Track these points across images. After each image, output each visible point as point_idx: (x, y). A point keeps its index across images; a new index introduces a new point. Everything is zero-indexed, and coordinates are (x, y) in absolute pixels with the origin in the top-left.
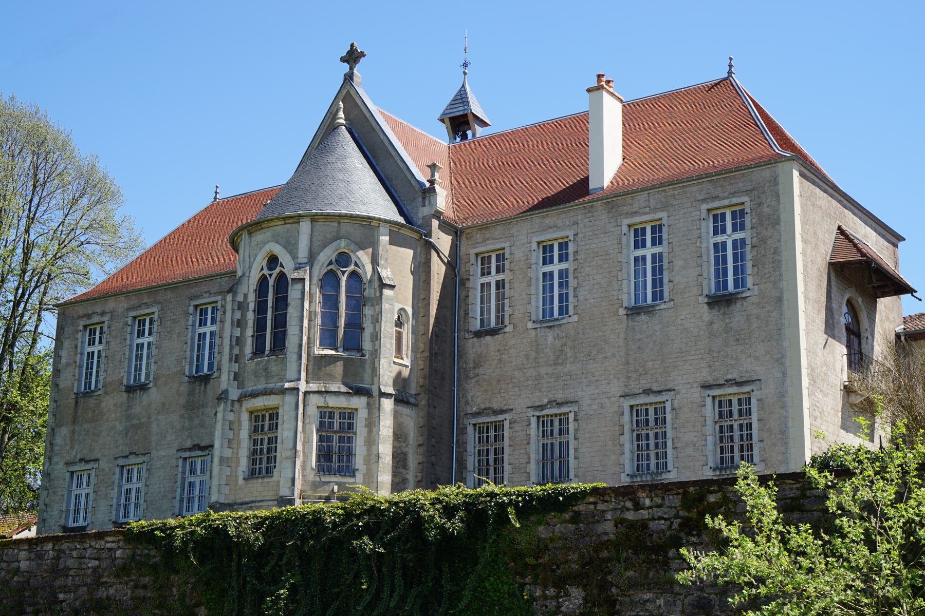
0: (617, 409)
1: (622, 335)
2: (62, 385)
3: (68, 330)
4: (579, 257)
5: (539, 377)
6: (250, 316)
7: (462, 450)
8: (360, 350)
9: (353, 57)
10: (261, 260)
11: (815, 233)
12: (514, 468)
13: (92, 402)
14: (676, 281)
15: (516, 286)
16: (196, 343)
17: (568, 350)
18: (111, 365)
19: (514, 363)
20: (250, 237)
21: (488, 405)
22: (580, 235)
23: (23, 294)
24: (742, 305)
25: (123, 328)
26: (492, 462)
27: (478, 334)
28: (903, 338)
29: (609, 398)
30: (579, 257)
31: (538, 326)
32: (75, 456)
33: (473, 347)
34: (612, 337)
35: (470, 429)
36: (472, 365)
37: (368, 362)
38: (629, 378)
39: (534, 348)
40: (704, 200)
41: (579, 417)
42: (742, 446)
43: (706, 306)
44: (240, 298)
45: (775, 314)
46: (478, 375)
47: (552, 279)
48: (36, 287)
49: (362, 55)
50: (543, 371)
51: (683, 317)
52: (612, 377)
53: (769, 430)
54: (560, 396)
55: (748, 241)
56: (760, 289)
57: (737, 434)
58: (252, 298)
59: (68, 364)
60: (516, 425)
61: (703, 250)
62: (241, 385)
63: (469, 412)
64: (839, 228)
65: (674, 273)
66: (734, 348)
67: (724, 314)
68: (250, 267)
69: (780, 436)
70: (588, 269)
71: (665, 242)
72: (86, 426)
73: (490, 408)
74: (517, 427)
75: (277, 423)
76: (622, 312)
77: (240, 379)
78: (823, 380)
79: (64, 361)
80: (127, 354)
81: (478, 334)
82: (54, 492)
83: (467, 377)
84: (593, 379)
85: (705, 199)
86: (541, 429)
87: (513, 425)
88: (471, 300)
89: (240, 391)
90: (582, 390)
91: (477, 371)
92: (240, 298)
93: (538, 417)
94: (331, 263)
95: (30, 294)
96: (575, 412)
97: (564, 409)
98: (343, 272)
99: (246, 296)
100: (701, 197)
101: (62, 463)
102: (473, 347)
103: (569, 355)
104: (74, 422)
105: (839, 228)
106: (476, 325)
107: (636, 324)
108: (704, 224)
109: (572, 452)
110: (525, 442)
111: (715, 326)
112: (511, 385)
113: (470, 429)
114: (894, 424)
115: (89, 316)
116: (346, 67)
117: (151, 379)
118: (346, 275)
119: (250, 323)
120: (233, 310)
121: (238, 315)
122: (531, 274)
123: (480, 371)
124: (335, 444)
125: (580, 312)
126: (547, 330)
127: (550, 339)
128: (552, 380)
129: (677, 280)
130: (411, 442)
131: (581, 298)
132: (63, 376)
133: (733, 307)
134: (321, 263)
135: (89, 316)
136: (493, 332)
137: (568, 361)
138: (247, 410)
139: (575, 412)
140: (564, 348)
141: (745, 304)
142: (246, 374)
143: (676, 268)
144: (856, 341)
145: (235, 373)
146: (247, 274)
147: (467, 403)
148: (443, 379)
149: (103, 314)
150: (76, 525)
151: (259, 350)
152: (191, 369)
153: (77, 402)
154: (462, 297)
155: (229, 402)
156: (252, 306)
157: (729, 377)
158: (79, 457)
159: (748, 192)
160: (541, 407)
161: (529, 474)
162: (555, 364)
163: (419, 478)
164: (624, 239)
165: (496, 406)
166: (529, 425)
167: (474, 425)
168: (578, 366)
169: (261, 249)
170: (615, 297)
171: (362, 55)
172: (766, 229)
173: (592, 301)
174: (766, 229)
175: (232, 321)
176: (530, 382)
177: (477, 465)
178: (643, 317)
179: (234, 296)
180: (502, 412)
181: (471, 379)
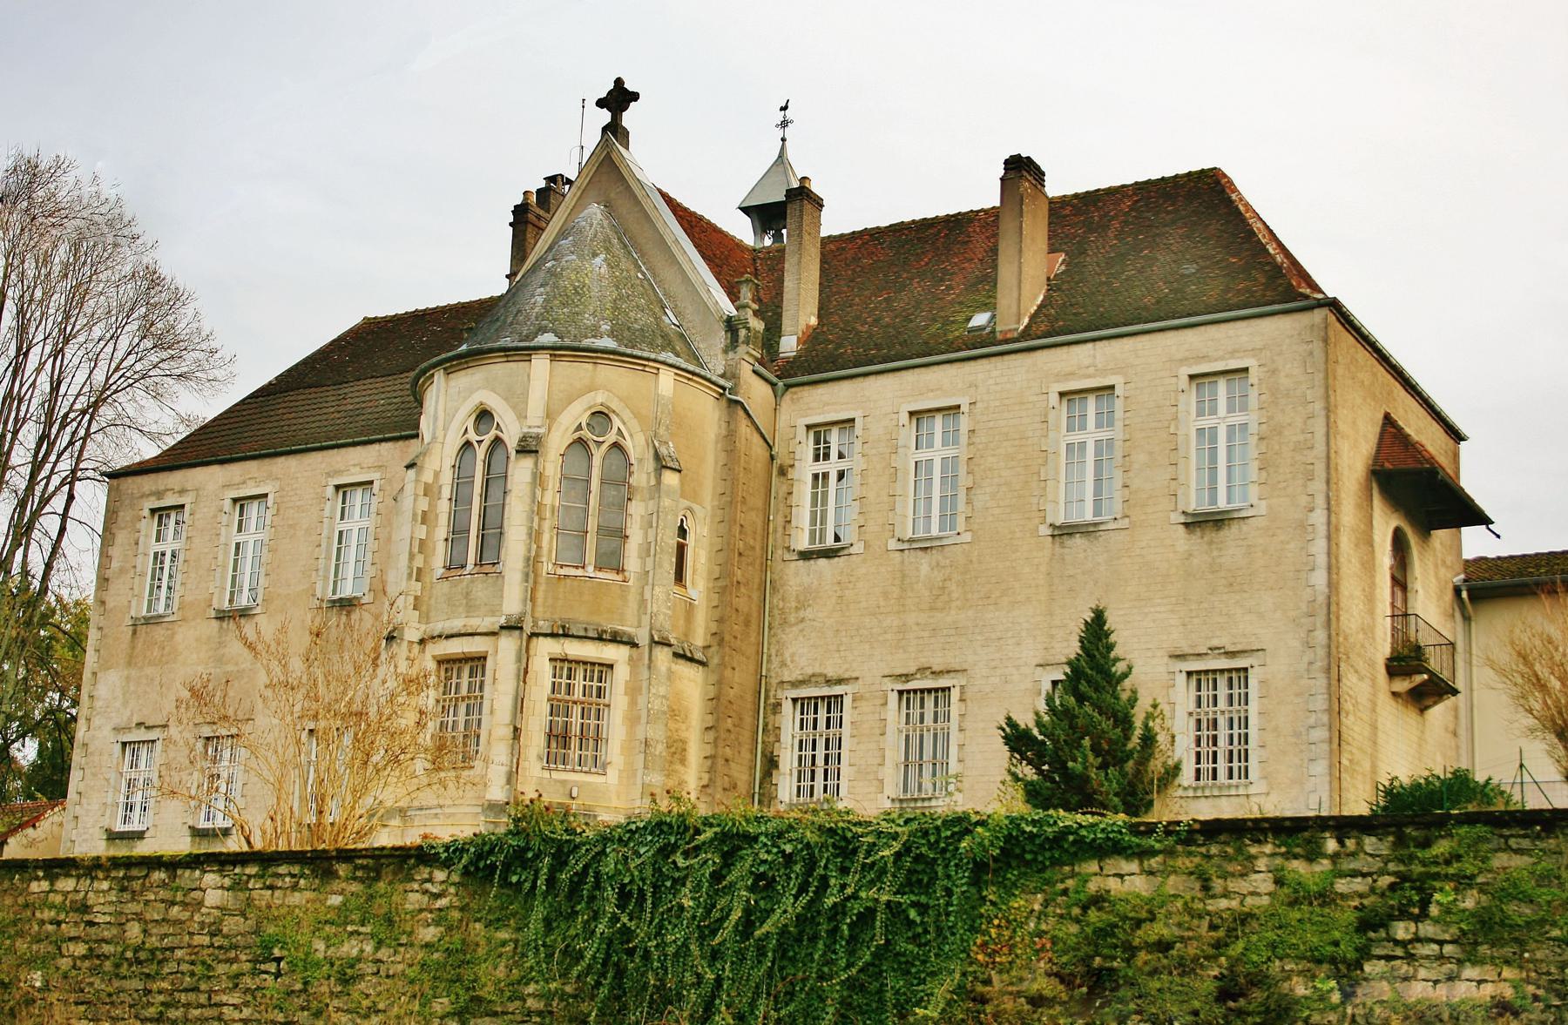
0: (1030, 685)
1: (1043, 569)
2: (110, 604)
3: (125, 515)
4: (977, 440)
5: (903, 629)
6: (444, 507)
7: (772, 739)
8: (620, 570)
9: (619, 99)
10: (463, 418)
11: (1354, 422)
12: (859, 772)
13: (159, 633)
14: (1133, 487)
15: (871, 480)
16: (336, 545)
17: (954, 587)
18: (193, 575)
19: (864, 605)
20: (447, 381)
21: (817, 670)
22: (979, 405)
23: (47, 454)
24: (1240, 530)
25: (215, 516)
26: (820, 761)
27: (806, 556)
28: (1464, 595)
29: (1018, 667)
30: (977, 440)
31: (906, 546)
32: (130, 719)
33: (797, 576)
34: (1027, 570)
35: (787, 706)
36: (794, 604)
37: (633, 590)
38: (1052, 637)
39: (897, 582)
40: (1184, 361)
41: (968, 695)
42: (1231, 752)
43: (1181, 529)
44: (428, 477)
45: (1292, 546)
46: (802, 620)
47: (930, 471)
48: (71, 443)
49: (635, 97)
50: (911, 619)
51: (1144, 544)
52: (1024, 634)
53: (1276, 729)
54: (937, 663)
55: (1253, 428)
56: (1270, 507)
57: (1223, 733)
58: (447, 478)
59: (122, 571)
60: (864, 703)
61: (1180, 439)
62: (425, 618)
63: (786, 679)
64: (1387, 417)
65: (1131, 474)
66: (1225, 597)
67: (1211, 543)
68: (446, 429)
69: (1294, 740)
70: (990, 459)
71: (1119, 424)
72: (149, 671)
73: (820, 675)
74: (865, 706)
75: (482, 683)
76: (1045, 530)
77: (424, 608)
78: (1359, 655)
79: (115, 565)
80: (220, 558)
81: (806, 556)
82: (94, 775)
83: (785, 622)
84: (993, 636)
85: (1187, 359)
86: (904, 711)
87: (857, 704)
88: (794, 500)
89: (423, 627)
90: (975, 653)
91: (801, 614)
92: (428, 477)
93: (901, 693)
94: (579, 428)
95: (59, 456)
96: (962, 687)
97: (837, 690)
98: (599, 444)
99: (437, 474)
100: (1179, 356)
101: (109, 727)
102: (797, 574)
103: (955, 595)
104: (129, 664)
105: (1387, 417)
106: (803, 543)
107: (1066, 551)
108: (1182, 397)
109: (953, 750)
110: (878, 732)
111: (1195, 561)
112: (857, 639)
113: (787, 706)
114: (279, 787)
115: (159, 495)
116: (605, 116)
117: (259, 601)
118: (604, 447)
119: (443, 520)
120: (416, 495)
121: (423, 504)
122: (897, 461)
123: (808, 613)
124: (576, 720)
125: (975, 527)
126: (920, 553)
127: (925, 569)
128: (926, 634)
129: (1136, 483)
130: (694, 723)
131: (978, 504)
132: (114, 587)
133: (1224, 533)
134: (563, 428)
135: (159, 495)
136: (829, 554)
137: (954, 605)
138: (434, 657)
139: (962, 687)
140: (948, 584)
141: (1245, 528)
142: (433, 601)
143: (1136, 466)
144: (1399, 594)
145: (416, 598)
146: (440, 439)
147: (783, 664)
148: (747, 623)
149: (182, 492)
150: (127, 828)
151: (454, 566)
152: (325, 588)
153: (134, 632)
154: (782, 494)
155: (405, 644)
156: (446, 492)
157: (1215, 643)
158: (136, 720)
159: (1255, 352)
160: (907, 677)
161: (882, 781)
162: (931, 609)
163: (705, 782)
164: (1052, 416)
165: (831, 673)
166: (886, 704)
167: (795, 700)
168: (970, 613)
169: (465, 399)
170: (1035, 508)
171: (635, 97)
172: (1283, 411)
173: (997, 511)
174: (1283, 411)
175: (415, 515)
176: (888, 636)
177: (796, 764)
178: (1078, 540)
179: (418, 474)
180: (840, 681)
181: (792, 625)
